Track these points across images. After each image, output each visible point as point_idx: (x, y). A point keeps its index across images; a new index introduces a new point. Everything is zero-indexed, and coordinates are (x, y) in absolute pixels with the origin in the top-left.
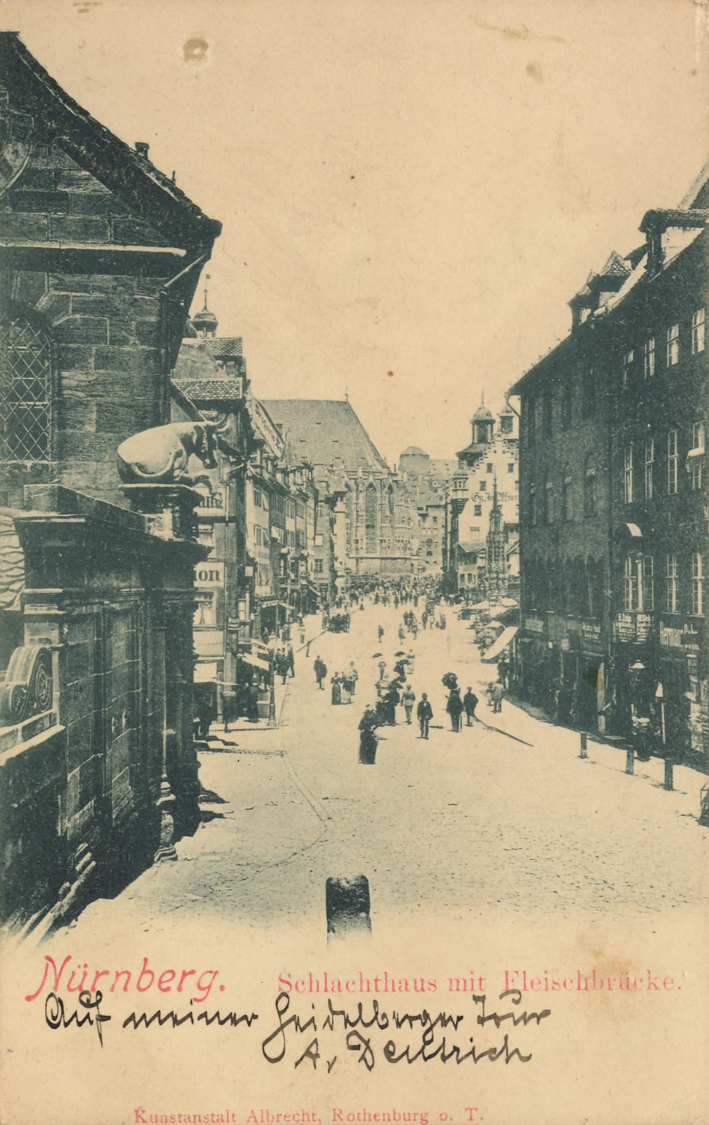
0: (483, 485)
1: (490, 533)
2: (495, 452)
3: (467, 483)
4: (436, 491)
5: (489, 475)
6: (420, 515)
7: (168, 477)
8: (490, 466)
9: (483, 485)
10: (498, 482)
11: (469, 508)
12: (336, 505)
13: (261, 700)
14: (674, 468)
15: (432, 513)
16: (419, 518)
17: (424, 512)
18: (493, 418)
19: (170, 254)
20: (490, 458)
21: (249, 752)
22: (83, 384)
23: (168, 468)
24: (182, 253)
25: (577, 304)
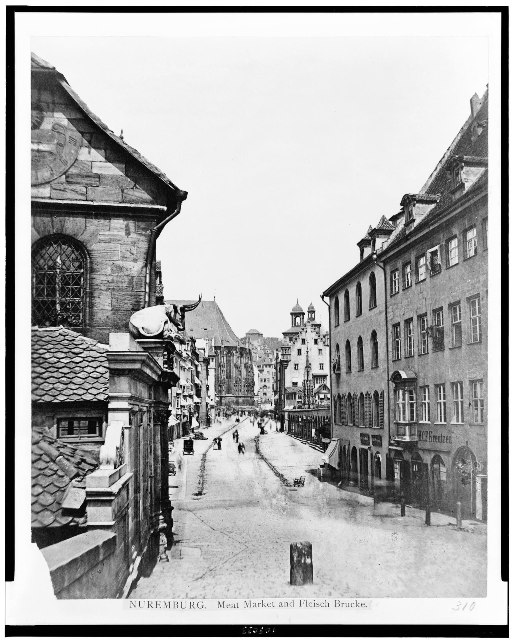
0: (299, 352)
1: (304, 381)
2: (306, 332)
3: (289, 350)
4: (268, 356)
5: (303, 346)
6: (259, 370)
7: (161, 335)
8: (303, 341)
9: (299, 352)
10: (309, 350)
11: (291, 366)
12: (209, 364)
13: (91, 521)
14: (457, 312)
15: (266, 369)
16: (259, 372)
17: (261, 368)
18: (304, 311)
19: (158, 209)
20: (303, 336)
21: (202, 476)
22: (105, 282)
23: (161, 330)
24: (165, 208)
25: (362, 244)
